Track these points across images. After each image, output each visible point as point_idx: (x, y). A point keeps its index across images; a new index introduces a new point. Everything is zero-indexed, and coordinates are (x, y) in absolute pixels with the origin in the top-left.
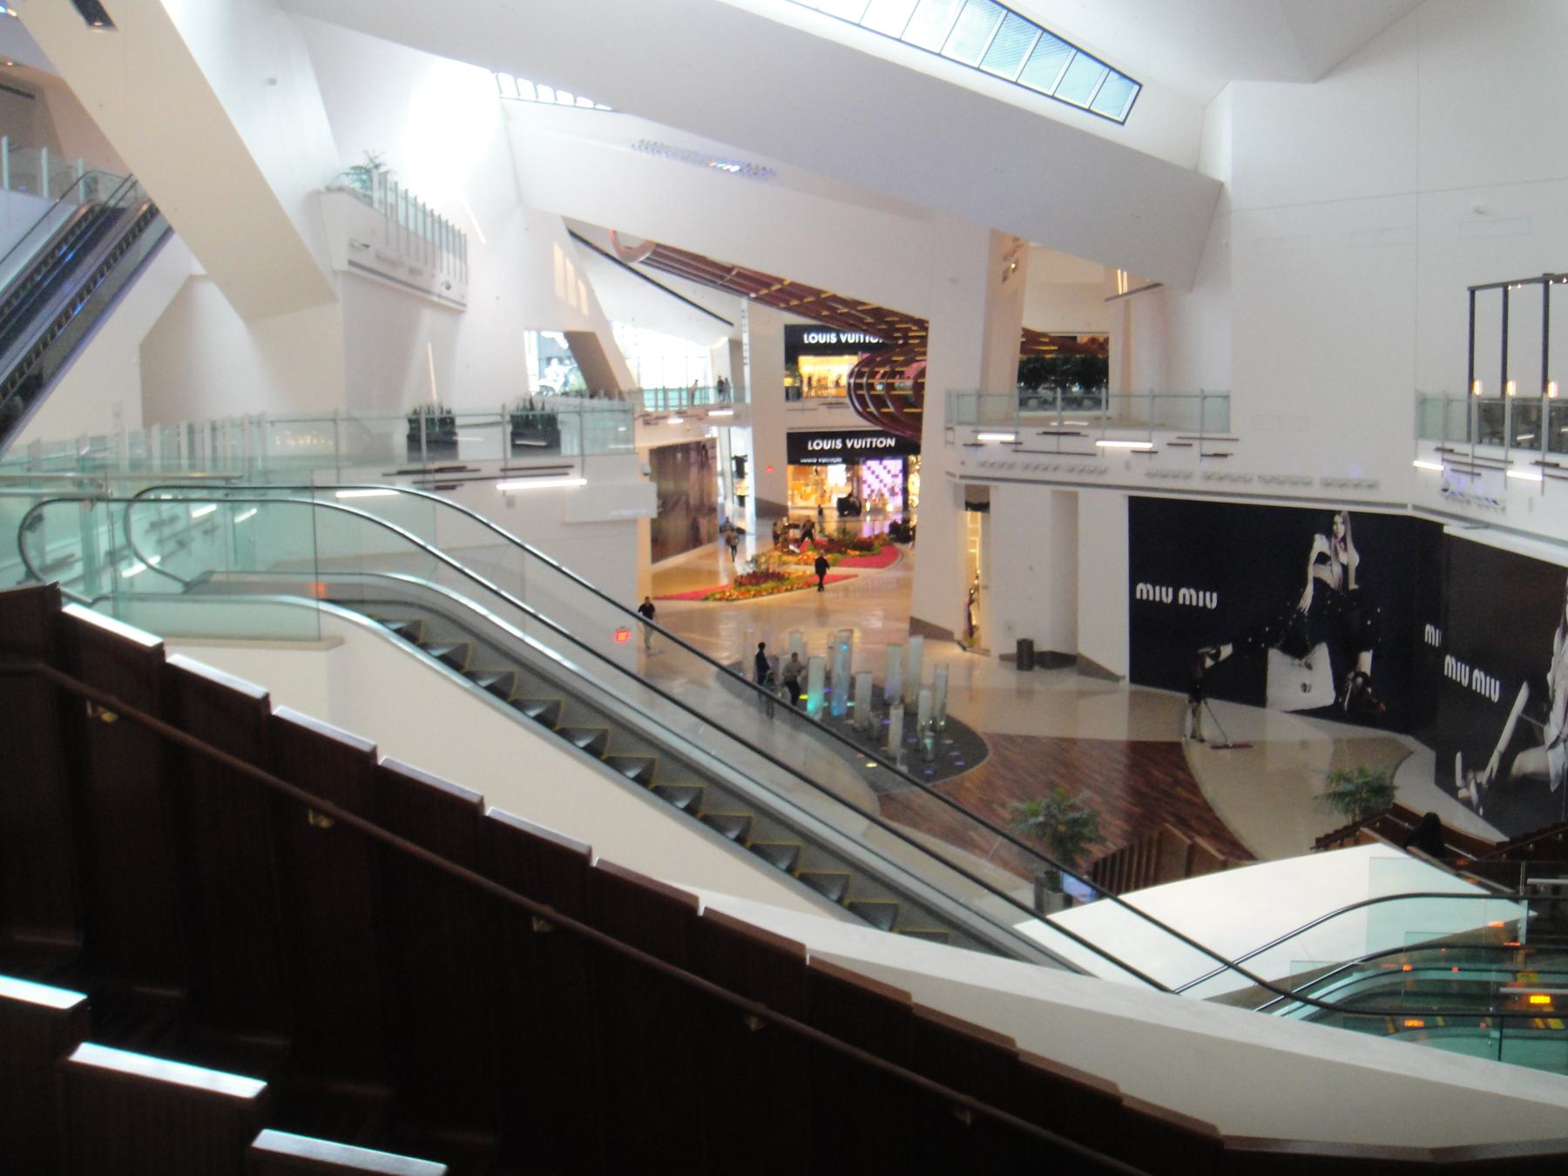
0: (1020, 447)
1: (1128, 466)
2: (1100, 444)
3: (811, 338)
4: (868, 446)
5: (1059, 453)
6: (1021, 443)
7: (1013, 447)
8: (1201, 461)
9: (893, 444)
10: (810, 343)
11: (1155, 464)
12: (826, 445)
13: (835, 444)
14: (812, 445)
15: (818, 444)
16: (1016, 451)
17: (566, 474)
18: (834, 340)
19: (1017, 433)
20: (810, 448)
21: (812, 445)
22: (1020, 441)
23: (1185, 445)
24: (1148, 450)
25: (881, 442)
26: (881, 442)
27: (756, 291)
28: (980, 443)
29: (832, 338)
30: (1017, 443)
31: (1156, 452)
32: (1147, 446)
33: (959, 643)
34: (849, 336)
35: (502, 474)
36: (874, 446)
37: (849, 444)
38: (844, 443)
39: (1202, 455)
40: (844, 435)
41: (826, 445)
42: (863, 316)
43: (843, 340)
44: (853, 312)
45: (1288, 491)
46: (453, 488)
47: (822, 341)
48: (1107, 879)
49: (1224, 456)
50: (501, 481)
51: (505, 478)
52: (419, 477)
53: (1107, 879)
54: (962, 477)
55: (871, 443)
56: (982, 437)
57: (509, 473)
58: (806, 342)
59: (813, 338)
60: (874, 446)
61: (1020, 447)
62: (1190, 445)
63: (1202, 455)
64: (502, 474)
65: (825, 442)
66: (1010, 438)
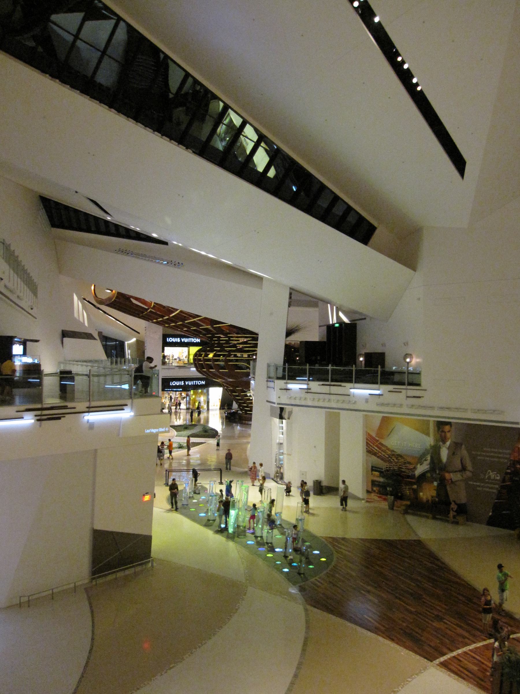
0: (309, 391)
1: (367, 401)
2: (352, 391)
3: (170, 340)
4: (194, 384)
5: (330, 394)
6: (310, 389)
7: (306, 391)
8: (406, 400)
9: (204, 383)
10: (169, 342)
11: (381, 400)
12: (178, 383)
13: (181, 383)
14: (172, 384)
15: (174, 383)
16: (307, 393)
17: (123, 409)
18: (179, 341)
19: (308, 384)
20: (171, 385)
21: (172, 384)
22: (309, 388)
23: (398, 392)
24: (378, 394)
25: (200, 383)
26: (200, 383)
27: (157, 319)
28: (288, 388)
29: (178, 340)
30: (308, 389)
31: (382, 395)
32: (377, 392)
33: (273, 479)
34: (185, 339)
35: (87, 410)
36: (196, 384)
37: (187, 383)
38: (185, 383)
39: (408, 397)
40: (185, 380)
41: (178, 383)
42: (202, 331)
43: (179, 339)
44: (189, 330)
45: (470, 415)
46: (59, 418)
47: (174, 341)
48: (317, 583)
49: (420, 397)
50: (87, 414)
51: (89, 412)
52: (39, 413)
53: (317, 583)
54: (278, 404)
55: (196, 383)
56: (290, 386)
57: (92, 409)
58: (168, 341)
59: (171, 340)
60: (196, 384)
61: (309, 391)
62: (401, 392)
63: (408, 397)
64: (87, 410)
65: (177, 382)
66: (305, 386)
